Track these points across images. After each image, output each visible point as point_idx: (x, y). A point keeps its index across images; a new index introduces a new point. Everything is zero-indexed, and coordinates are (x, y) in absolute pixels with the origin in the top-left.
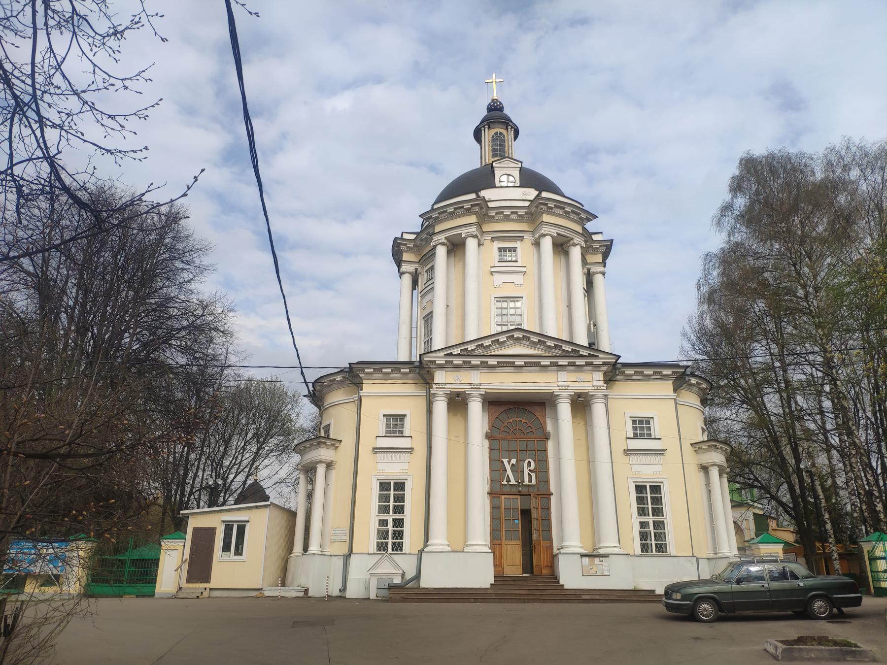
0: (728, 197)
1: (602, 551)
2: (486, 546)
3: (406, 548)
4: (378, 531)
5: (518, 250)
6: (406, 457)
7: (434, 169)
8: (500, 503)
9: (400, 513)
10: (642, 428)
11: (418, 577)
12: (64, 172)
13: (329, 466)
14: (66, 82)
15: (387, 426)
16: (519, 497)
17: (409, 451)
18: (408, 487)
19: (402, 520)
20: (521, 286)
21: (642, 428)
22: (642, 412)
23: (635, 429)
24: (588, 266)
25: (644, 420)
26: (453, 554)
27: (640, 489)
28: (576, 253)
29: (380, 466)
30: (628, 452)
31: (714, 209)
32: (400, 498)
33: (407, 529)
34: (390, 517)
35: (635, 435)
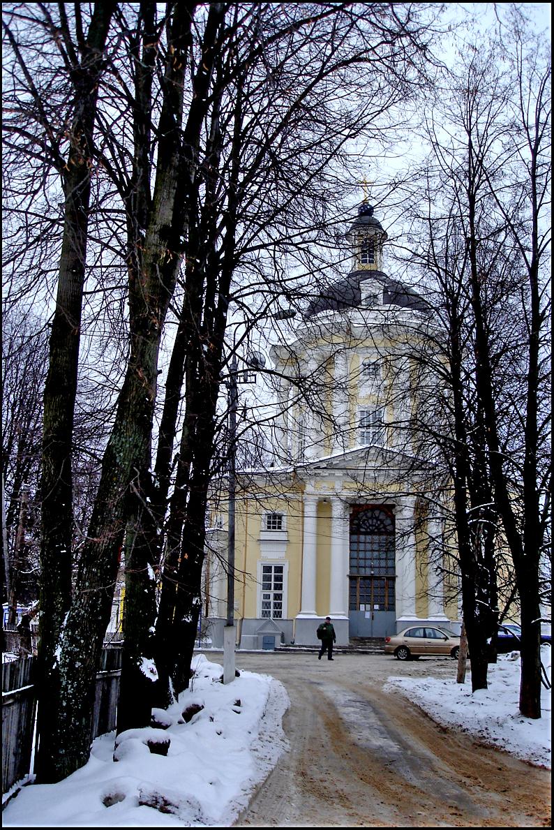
4: (263, 603)
7: (547, 28)
10: (274, 523)
12: (531, 137)
14: (521, 113)
19: (281, 595)
23: (280, 523)
25: (277, 530)
32: (279, 579)
33: (284, 601)
34: (272, 593)
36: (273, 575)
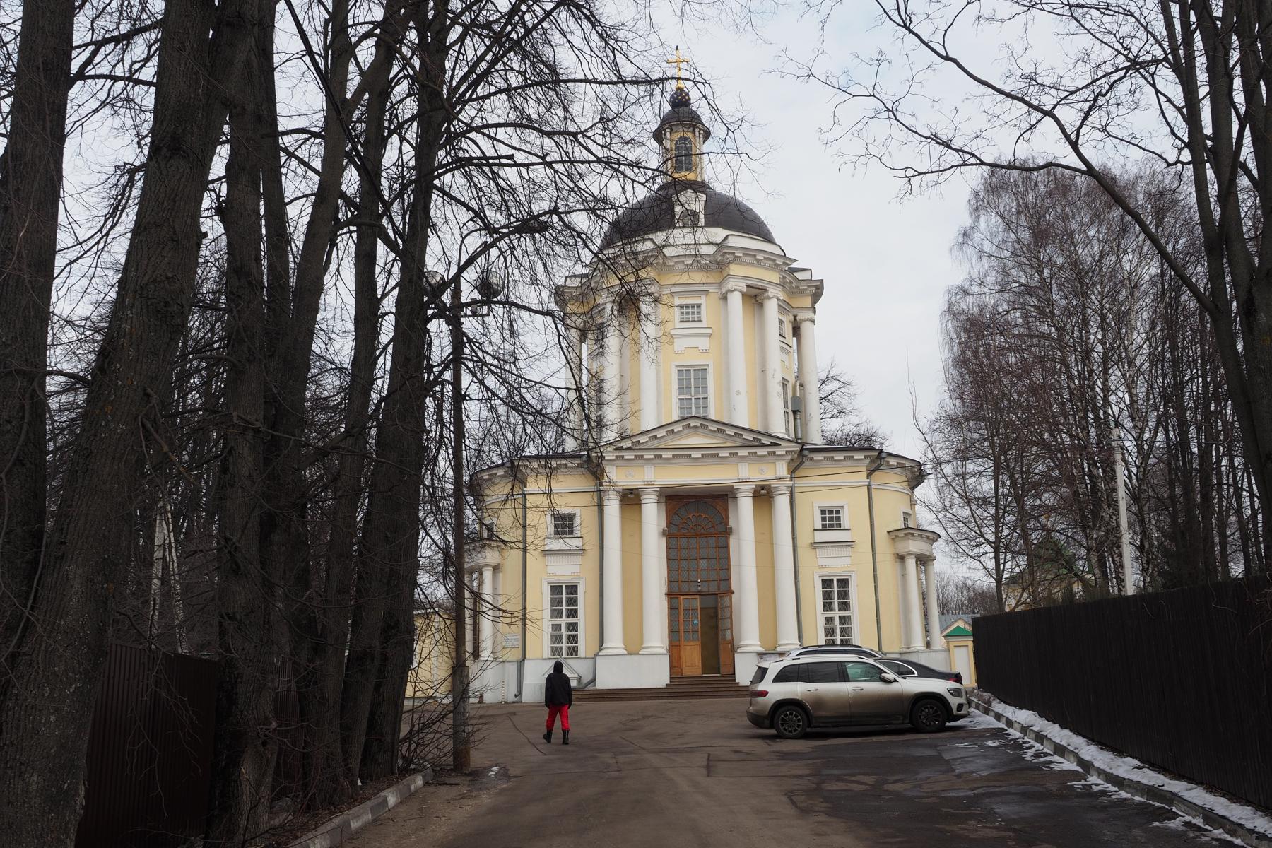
0: (967, 221)
1: (779, 649)
2: (663, 647)
3: (581, 653)
5: (703, 308)
6: (578, 559)
8: (679, 602)
9: (573, 617)
10: (831, 519)
11: (594, 680)
13: (496, 569)
15: (556, 526)
16: (698, 596)
17: (581, 551)
18: (581, 590)
19: (576, 624)
20: (705, 352)
21: (831, 519)
22: (831, 501)
23: (823, 519)
24: (795, 312)
26: (628, 657)
27: (827, 583)
28: (772, 308)
29: (550, 570)
30: (814, 545)
31: (951, 234)
32: (573, 602)
35: (824, 526)
36: (564, 596)
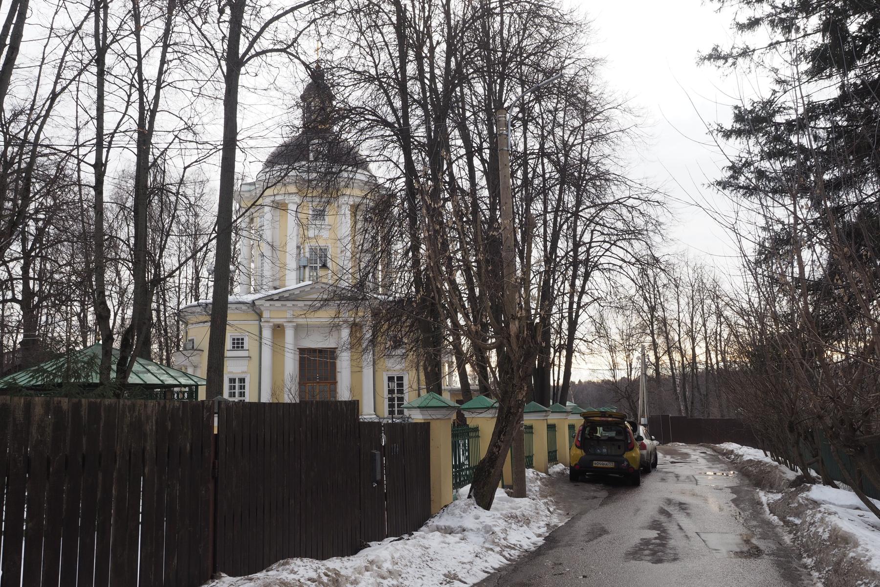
10: (238, 343)
23: (234, 343)
